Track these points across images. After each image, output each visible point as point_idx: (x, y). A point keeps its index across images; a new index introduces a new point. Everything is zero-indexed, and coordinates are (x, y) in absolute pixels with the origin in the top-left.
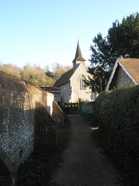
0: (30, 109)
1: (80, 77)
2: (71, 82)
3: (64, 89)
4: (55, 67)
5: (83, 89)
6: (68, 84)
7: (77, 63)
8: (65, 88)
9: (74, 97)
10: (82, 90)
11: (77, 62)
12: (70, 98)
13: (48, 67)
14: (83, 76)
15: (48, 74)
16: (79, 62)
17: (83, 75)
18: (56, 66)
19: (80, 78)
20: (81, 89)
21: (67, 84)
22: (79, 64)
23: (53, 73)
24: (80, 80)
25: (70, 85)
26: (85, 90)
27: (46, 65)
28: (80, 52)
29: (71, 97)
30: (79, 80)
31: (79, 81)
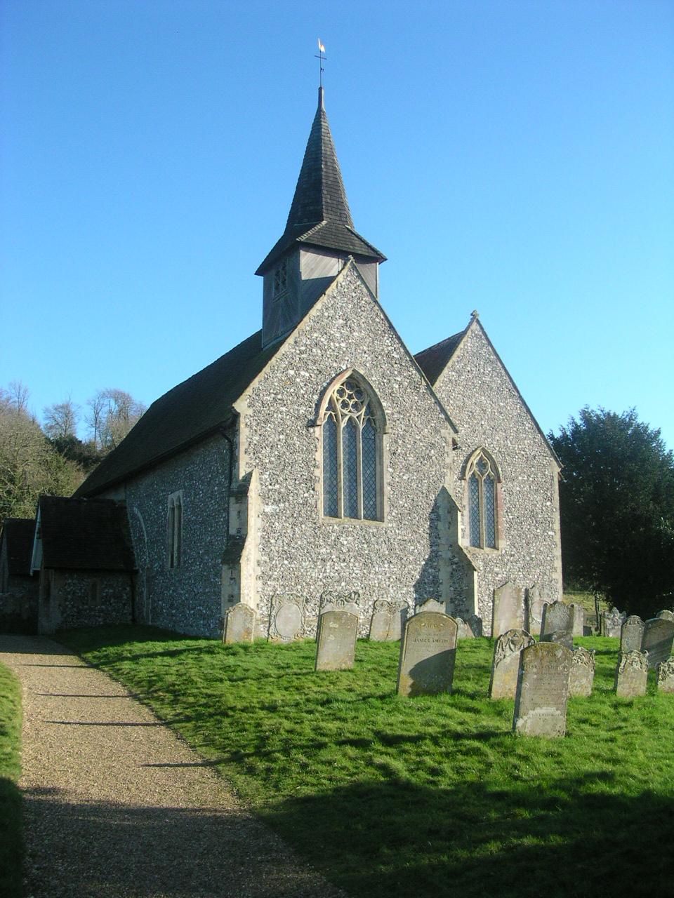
0: (628, 615)
1: (332, 392)
2: (245, 434)
3: (161, 502)
4: (103, 416)
5: (354, 514)
6: (217, 448)
7: (304, 277)
8: (175, 496)
9: (264, 577)
10: (346, 521)
11: (311, 265)
12: (226, 592)
13: (66, 411)
14: (359, 393)
15: (67, 447)
16: (331, 266)
17: (356, 385)
18: (114, 407)
19: (331, 406)
20: (333, 512)
21: (213, 452)
22: (323, 284)
23: (91, 446)
24: (332, 425)
25: (233, 460)
26: (374, 519)
27: (60, 404)
28: (336, 187)
29: (236, 580)
30: (323, 419)
31: (318, 432)
